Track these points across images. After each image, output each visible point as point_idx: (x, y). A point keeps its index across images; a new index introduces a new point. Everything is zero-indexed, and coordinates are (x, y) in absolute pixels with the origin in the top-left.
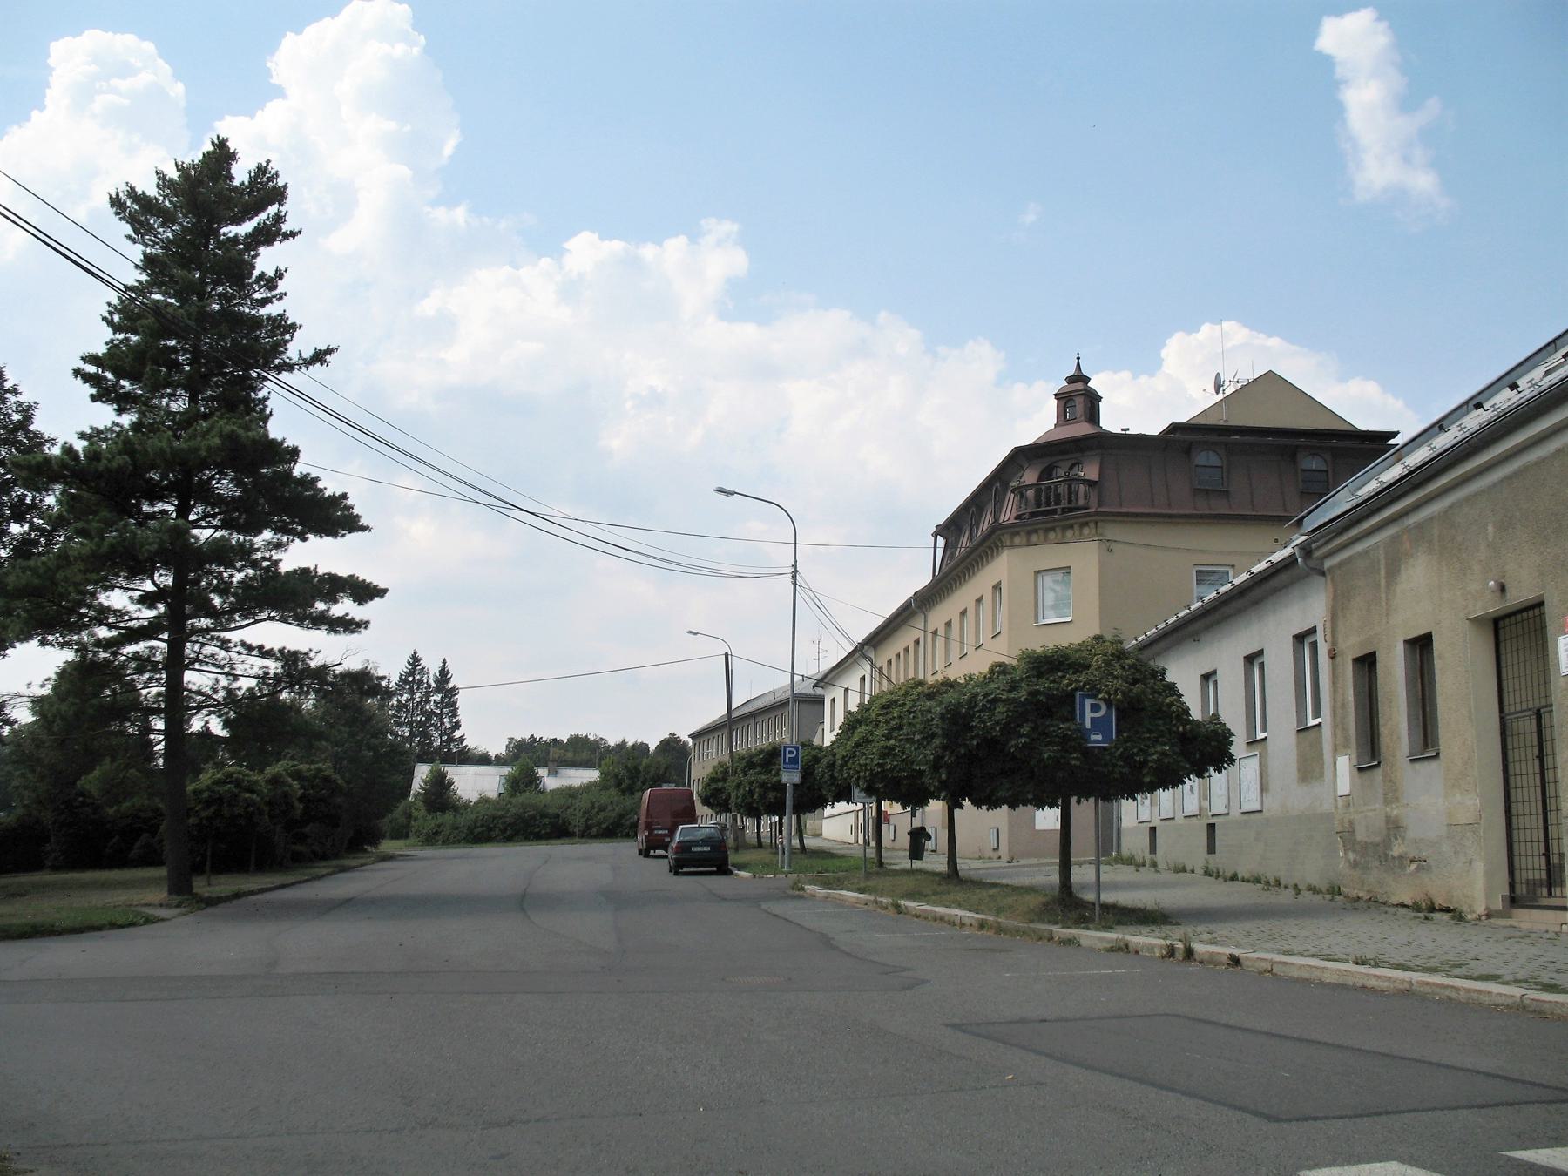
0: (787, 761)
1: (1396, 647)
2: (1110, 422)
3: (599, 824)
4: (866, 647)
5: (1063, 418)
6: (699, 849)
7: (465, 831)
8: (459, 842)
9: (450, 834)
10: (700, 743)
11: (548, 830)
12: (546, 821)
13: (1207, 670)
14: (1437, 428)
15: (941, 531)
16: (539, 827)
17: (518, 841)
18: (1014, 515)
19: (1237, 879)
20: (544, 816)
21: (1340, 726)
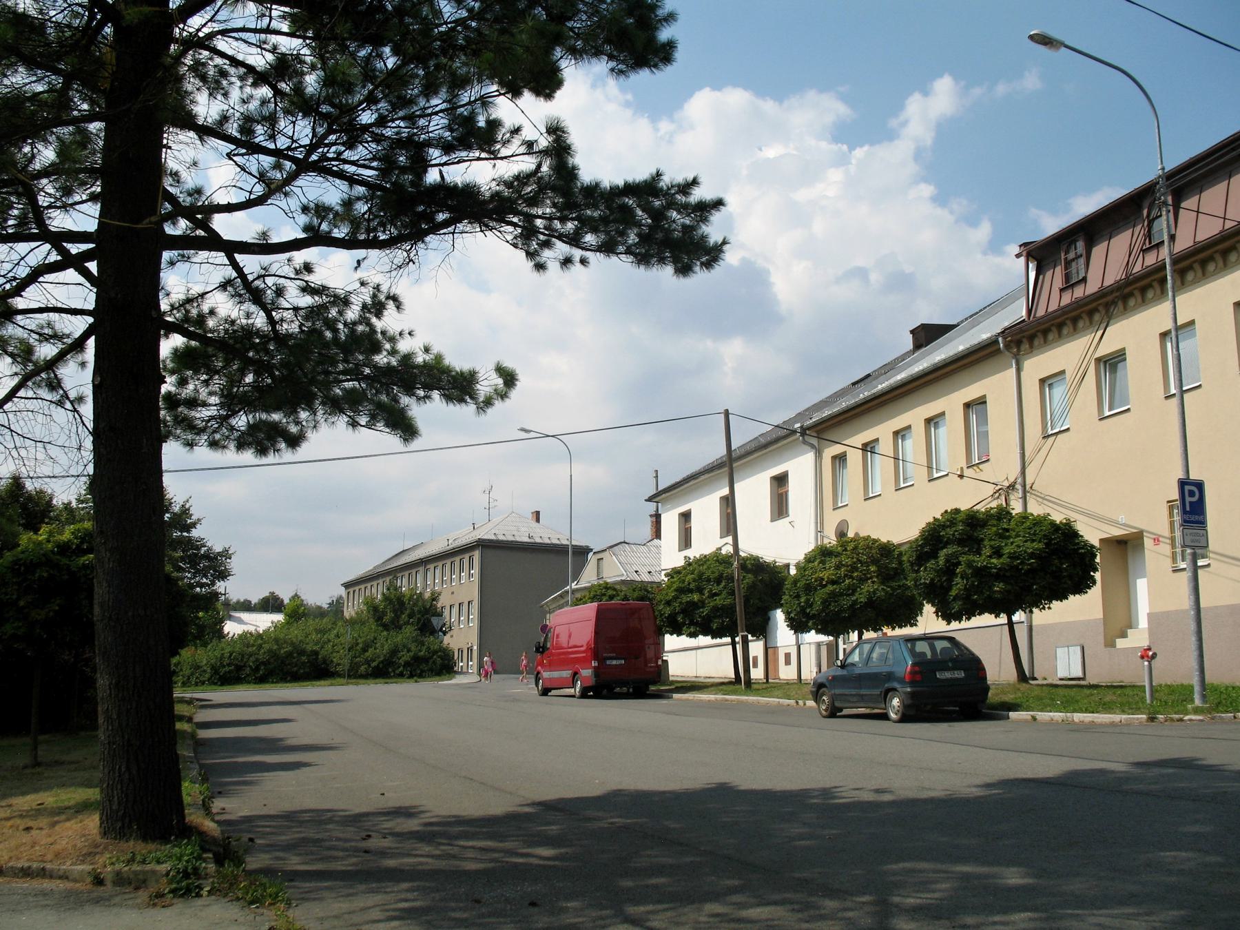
0: (1188, 509)
3: (368, 662)
6: (948, 675)
7: (209, 671)
8: (203, 683)
9: (192, 674)
10: (354, 592)
11: (307, 670)
12: (304, 658)
16: (296, 665)
17: (273, 682)
20: (302, 652)
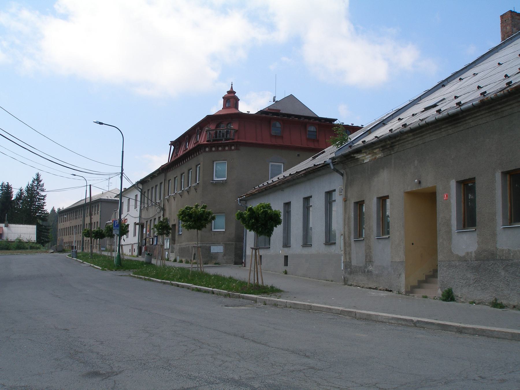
0: (116, 226)
1: (373, 199)
2: (243, 108)
4: (139, 184)
5: (225, 107)
13: (287, 201)
14: (381, 124)
15: (173, 143)
18: (206, 140)
19: (377, 289)
21: (347, 225)
